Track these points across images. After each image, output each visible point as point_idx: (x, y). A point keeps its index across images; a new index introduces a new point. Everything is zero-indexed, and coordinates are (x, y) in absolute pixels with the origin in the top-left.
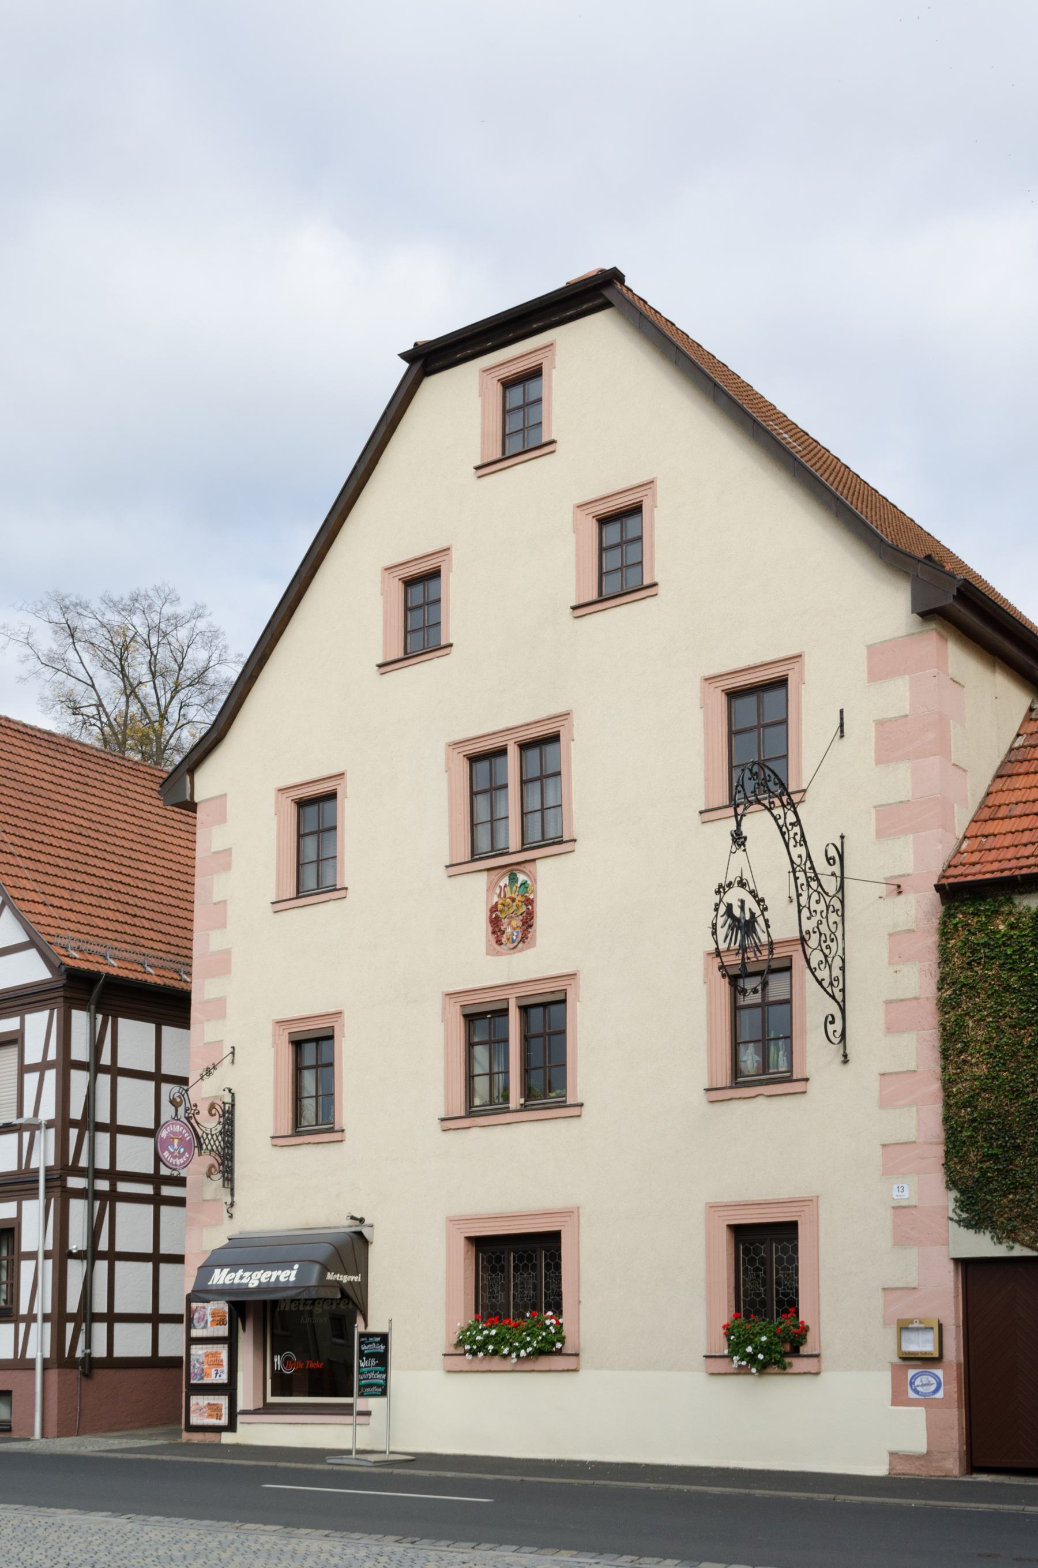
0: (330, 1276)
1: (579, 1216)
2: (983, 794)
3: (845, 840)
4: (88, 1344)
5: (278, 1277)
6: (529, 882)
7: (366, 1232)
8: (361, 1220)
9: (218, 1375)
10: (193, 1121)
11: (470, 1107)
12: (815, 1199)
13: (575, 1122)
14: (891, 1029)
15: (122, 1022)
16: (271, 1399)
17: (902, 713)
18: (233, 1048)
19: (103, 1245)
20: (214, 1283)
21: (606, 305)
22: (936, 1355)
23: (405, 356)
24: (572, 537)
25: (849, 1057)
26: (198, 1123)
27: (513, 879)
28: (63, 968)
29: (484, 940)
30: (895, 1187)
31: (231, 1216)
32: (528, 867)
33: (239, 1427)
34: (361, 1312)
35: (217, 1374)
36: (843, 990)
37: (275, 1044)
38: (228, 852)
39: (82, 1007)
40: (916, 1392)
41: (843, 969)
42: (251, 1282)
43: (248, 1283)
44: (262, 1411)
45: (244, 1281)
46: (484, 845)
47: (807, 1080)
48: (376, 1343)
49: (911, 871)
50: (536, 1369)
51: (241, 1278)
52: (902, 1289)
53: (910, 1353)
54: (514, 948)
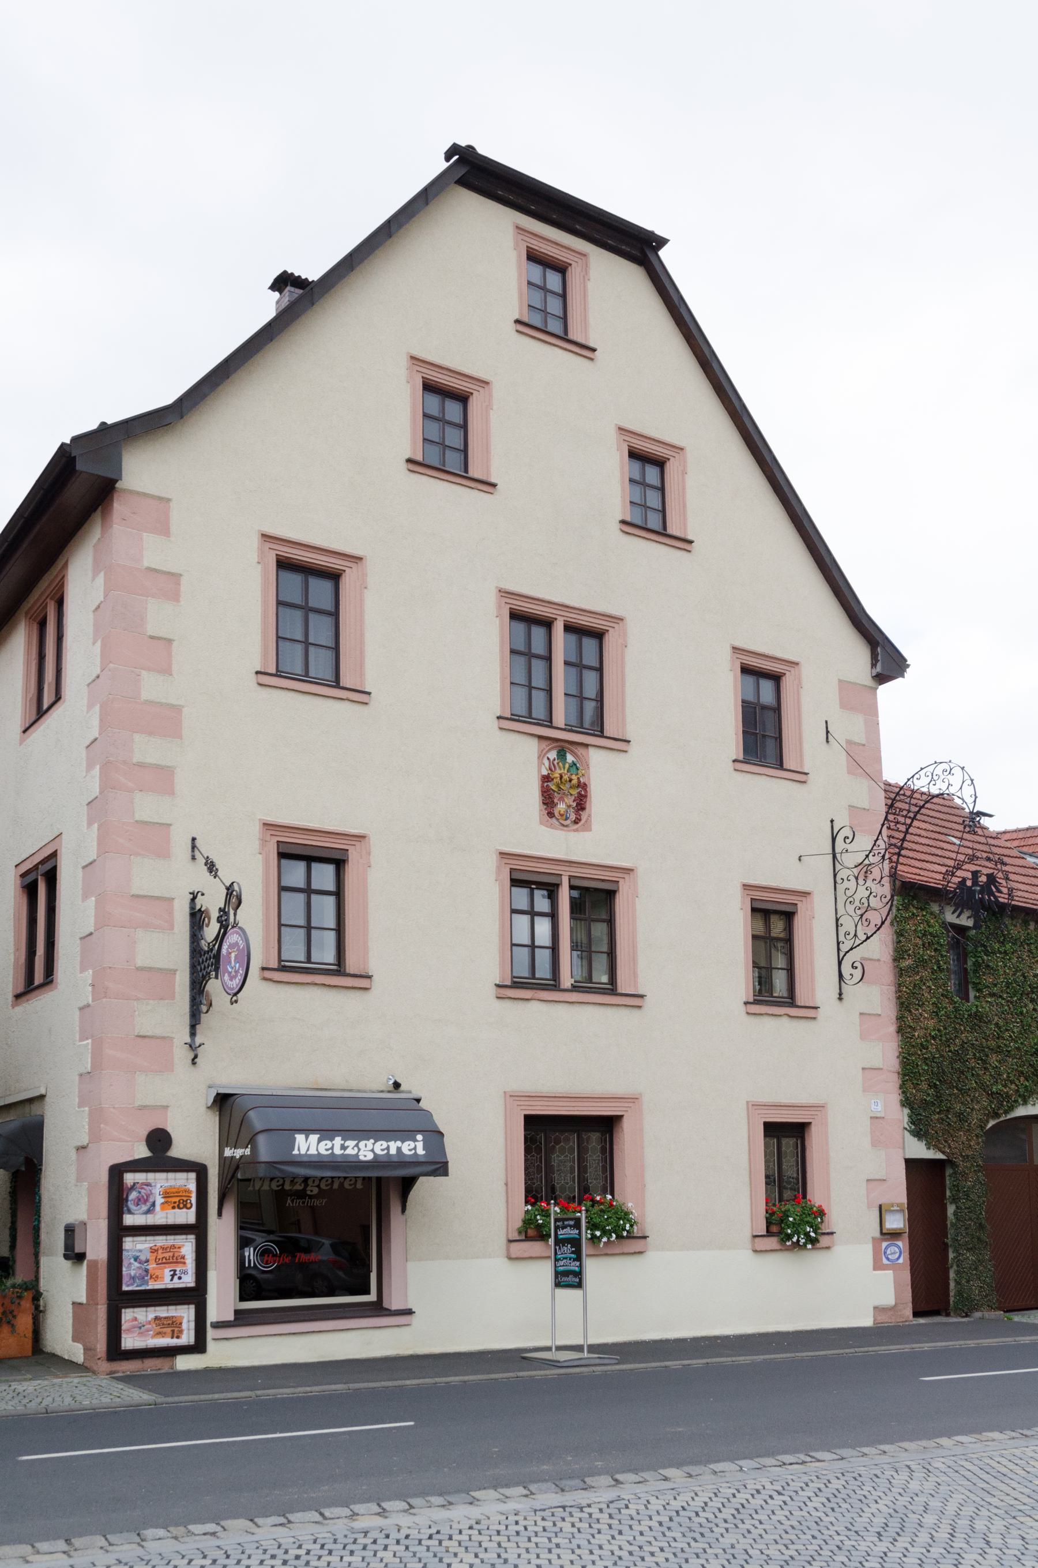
5: (399, 1149)
9: (176, 1278)
13: (635, 1012)
30: (873, 1101)
32: (580, 751)
33: (211, 1345)
35: (173, 1276)
40: (888, 1259)
48: (571, 1226)
50: (609, 1252)
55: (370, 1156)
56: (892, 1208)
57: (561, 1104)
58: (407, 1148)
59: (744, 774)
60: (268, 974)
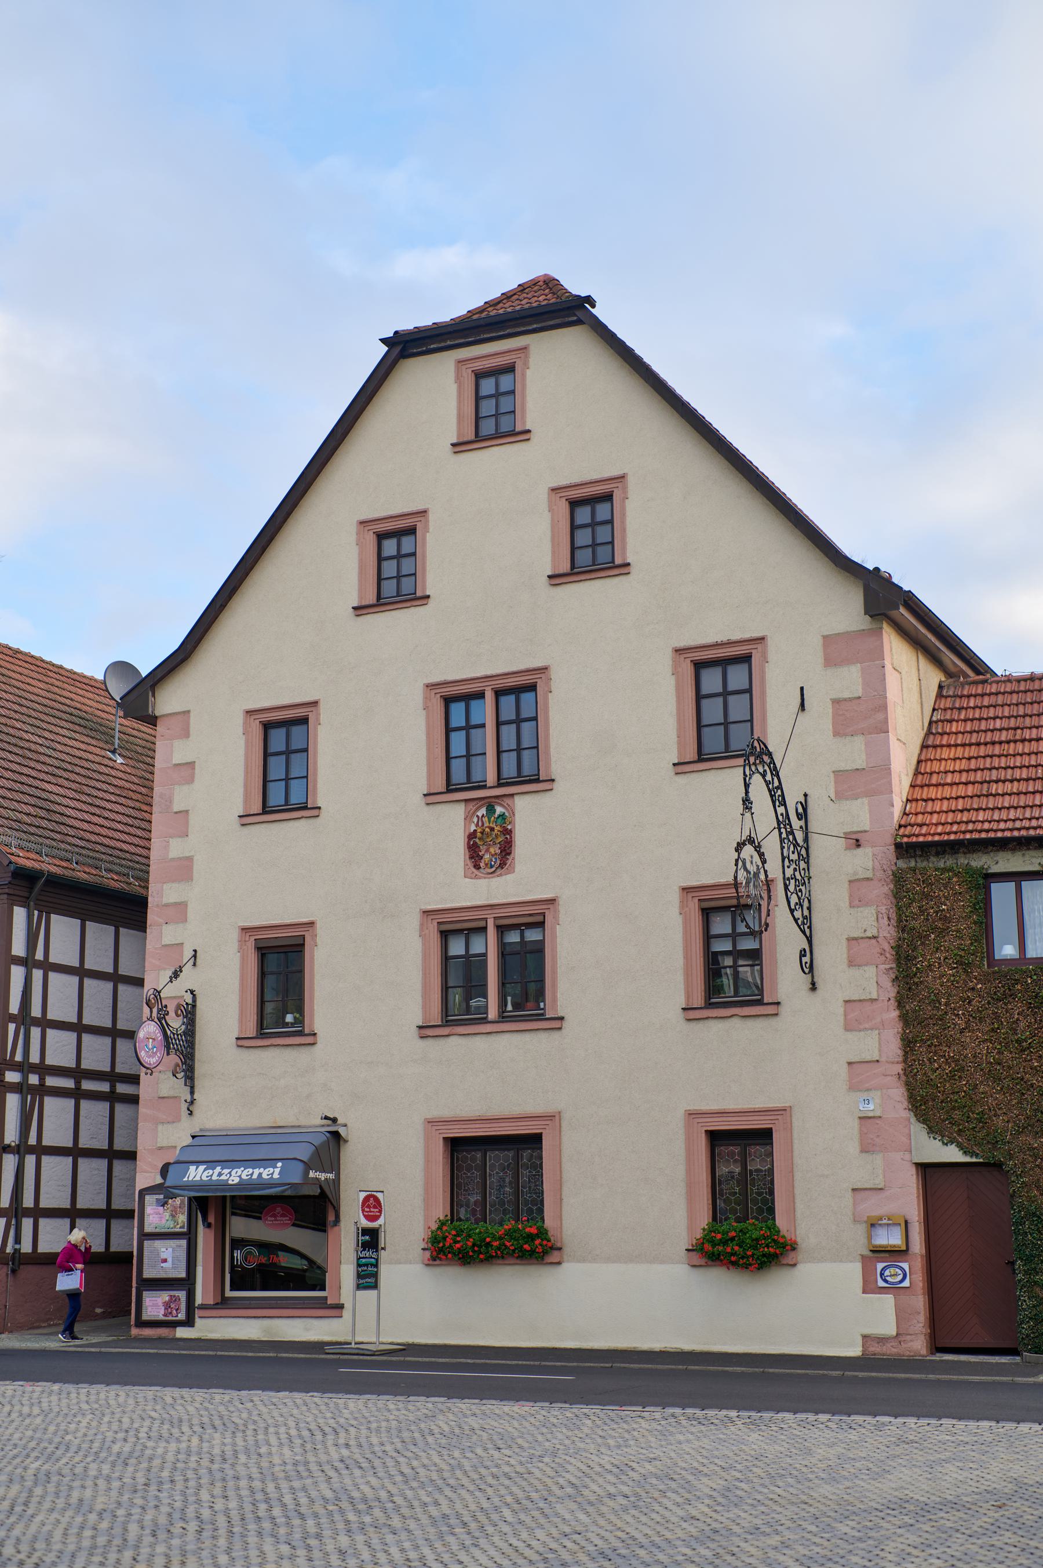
0: (312, 1174)
1: (560, 1120)
2: (915, 762)
3: (808, 798)
4: (18, 1240)
5: (260, 1174)
6: (507, 814)
7: (342, 1131)
8: (334, 1120)
10: (163, 1022)
11: (447, 1016)
12: (788, 1109)
13: (556, 1035)
14: (852, 963)
15: (54, 917)
16: (229, 1294)
17: (856, 695)
18: (195, 951)
19: (32, 1141)
20: (190, 1179)
21: (579, 322)
22: (904, 1248)
23: (384, 341)
24: (547, 516)
25: (817, 985)
26: (168, 1025)
27: (491, 810)
28: (12, 867)
29: (462, 864)
31: (191, 1113)
32: (508, 801)
33: (198, 1322)
34: (334, 1207)
36: (810, 927)
37: (240, 949)
38: (191, 765)
39: (24, 904)
40: (886, 1281)
41: (809, 908)
42: (231, 1178)
43: (228, 1180)
44: (219, 1306)
45: (223, 1177)
46: (459, 775)
47: (778, 1003)
49: (867, 828)
51: (220, 1174)
52: (870, 1189)
53: (880, 1246)
54: (491, 873)
55: (237, 1180)
56: (880, 1222)
57: (477, 1126)
58: (266, 1173)
59: (688, 774)
60: (692, 1014)
